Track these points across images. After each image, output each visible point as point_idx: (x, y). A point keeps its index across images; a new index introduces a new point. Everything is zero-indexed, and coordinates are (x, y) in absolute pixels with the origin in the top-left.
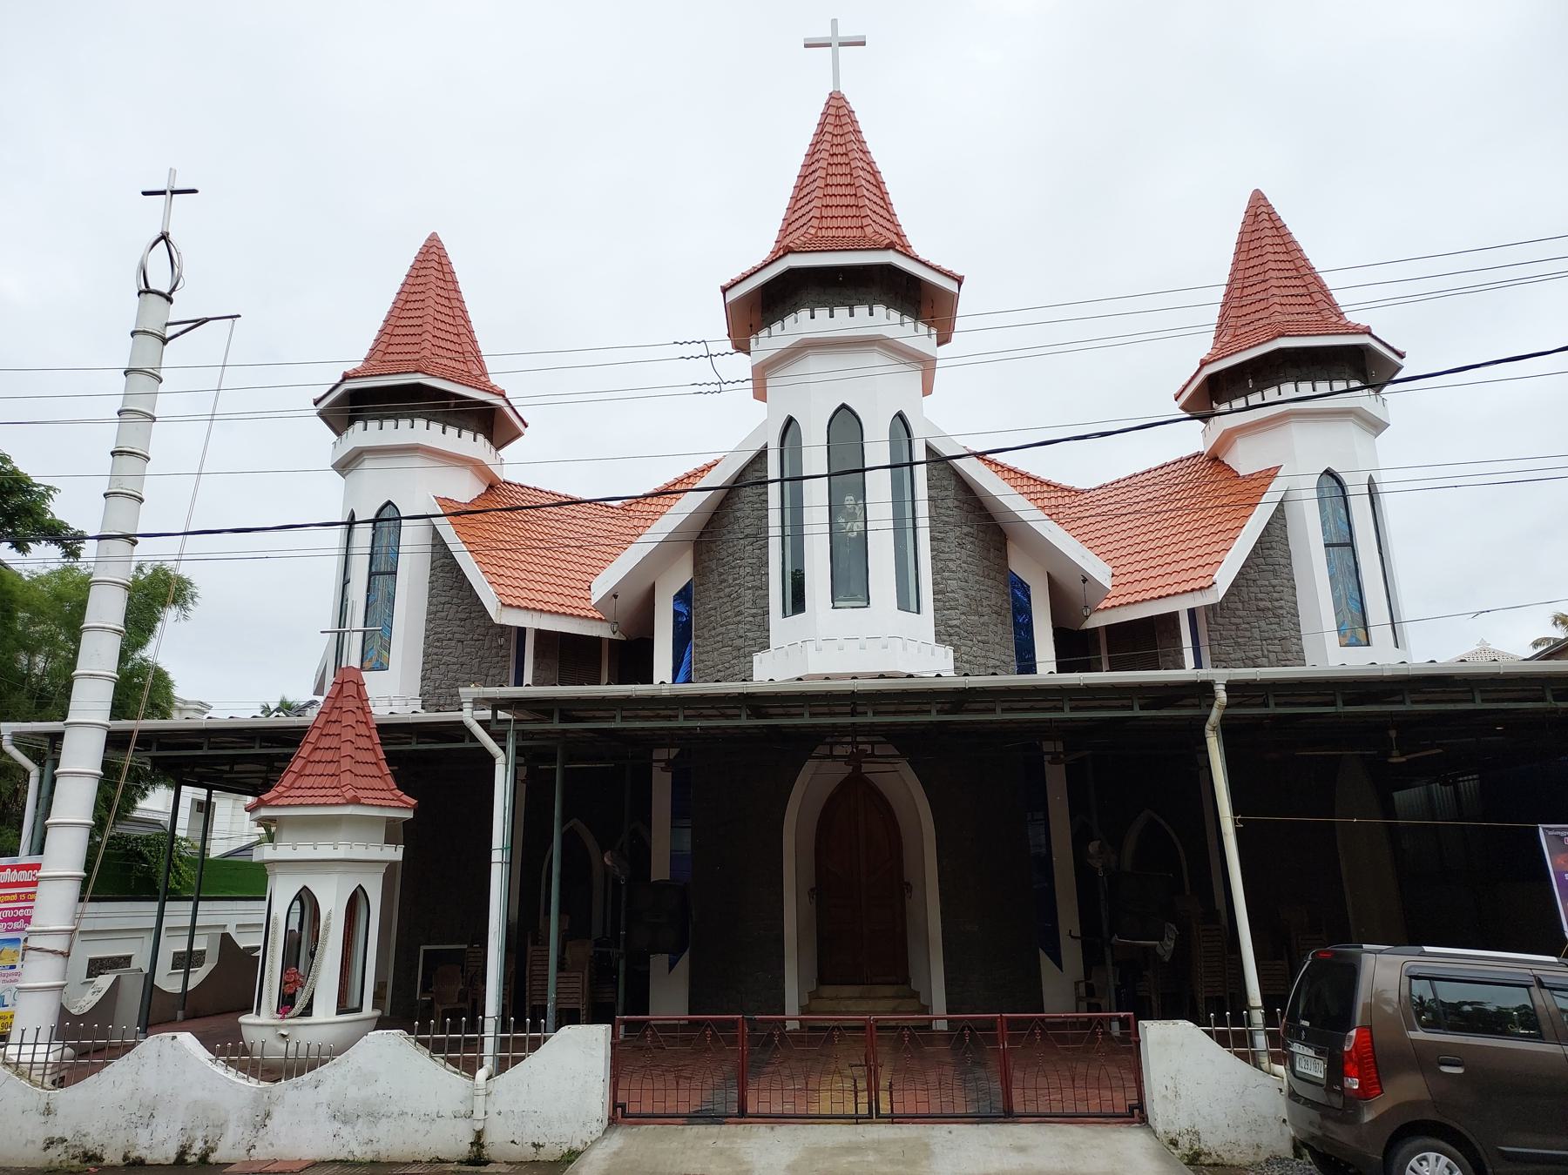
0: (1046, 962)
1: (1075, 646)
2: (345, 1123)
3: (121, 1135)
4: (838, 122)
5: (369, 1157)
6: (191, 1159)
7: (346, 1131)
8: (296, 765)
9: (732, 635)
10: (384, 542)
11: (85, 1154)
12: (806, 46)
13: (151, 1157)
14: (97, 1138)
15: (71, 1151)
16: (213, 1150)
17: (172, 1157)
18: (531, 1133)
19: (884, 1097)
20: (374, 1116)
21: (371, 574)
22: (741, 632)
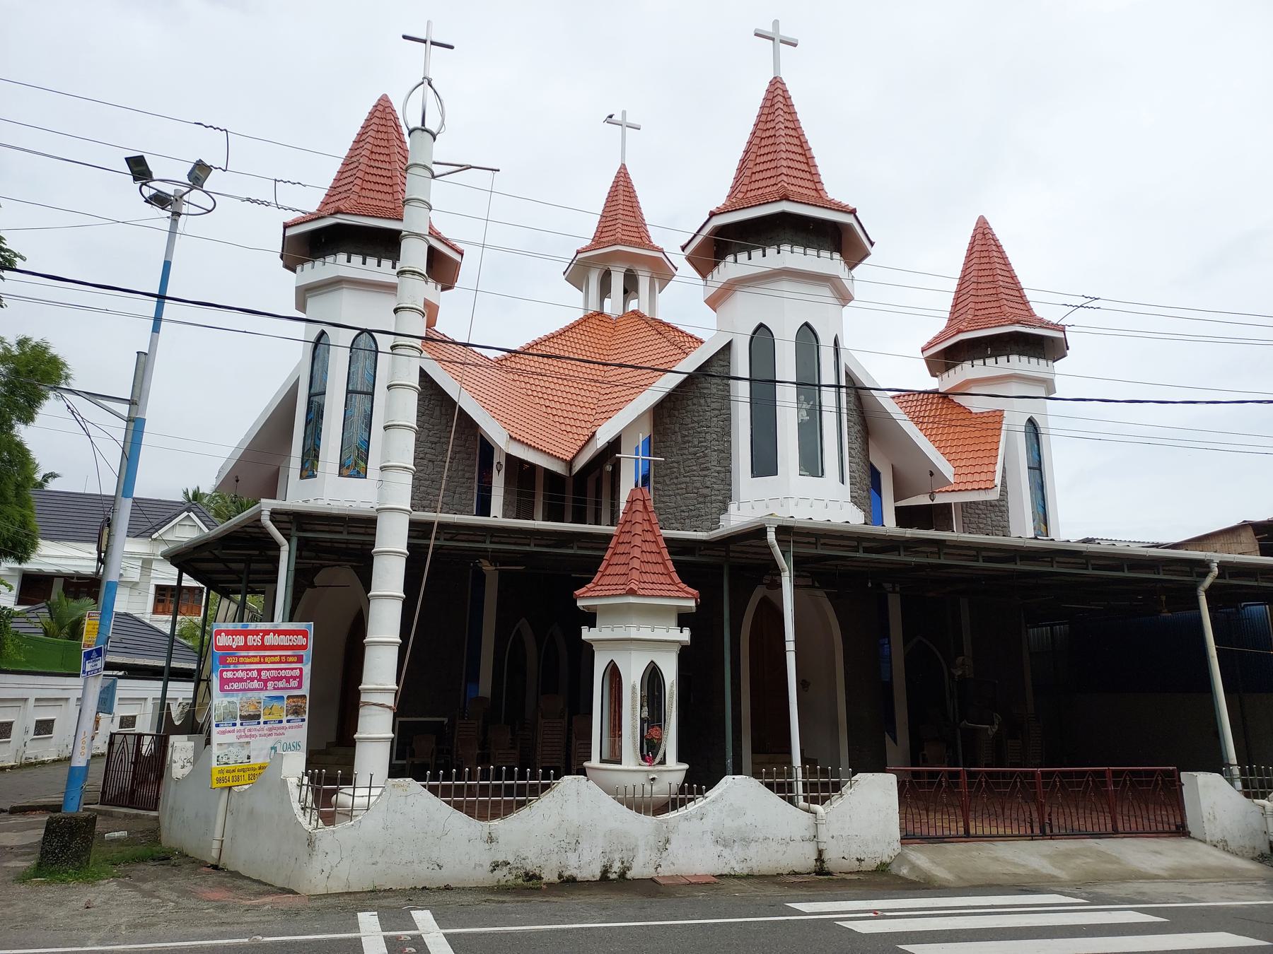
0: (888, 738)
1: (905, 517)
2: (725, 846)
3: (554, 858)
4: (777, 103)
5: (745, 872)
7: (726, 852)
9: (698, 485)
10: (360, 364)
11: (527, 874)
12: (756, 35)
13: (582, 875)
14: (535, 861)
15: (514, 872)
17: (598, 875)
18: (855, 851)
19: (972, 824)
20: (746, 841)
21: (348, 392)
22: (708, 484)
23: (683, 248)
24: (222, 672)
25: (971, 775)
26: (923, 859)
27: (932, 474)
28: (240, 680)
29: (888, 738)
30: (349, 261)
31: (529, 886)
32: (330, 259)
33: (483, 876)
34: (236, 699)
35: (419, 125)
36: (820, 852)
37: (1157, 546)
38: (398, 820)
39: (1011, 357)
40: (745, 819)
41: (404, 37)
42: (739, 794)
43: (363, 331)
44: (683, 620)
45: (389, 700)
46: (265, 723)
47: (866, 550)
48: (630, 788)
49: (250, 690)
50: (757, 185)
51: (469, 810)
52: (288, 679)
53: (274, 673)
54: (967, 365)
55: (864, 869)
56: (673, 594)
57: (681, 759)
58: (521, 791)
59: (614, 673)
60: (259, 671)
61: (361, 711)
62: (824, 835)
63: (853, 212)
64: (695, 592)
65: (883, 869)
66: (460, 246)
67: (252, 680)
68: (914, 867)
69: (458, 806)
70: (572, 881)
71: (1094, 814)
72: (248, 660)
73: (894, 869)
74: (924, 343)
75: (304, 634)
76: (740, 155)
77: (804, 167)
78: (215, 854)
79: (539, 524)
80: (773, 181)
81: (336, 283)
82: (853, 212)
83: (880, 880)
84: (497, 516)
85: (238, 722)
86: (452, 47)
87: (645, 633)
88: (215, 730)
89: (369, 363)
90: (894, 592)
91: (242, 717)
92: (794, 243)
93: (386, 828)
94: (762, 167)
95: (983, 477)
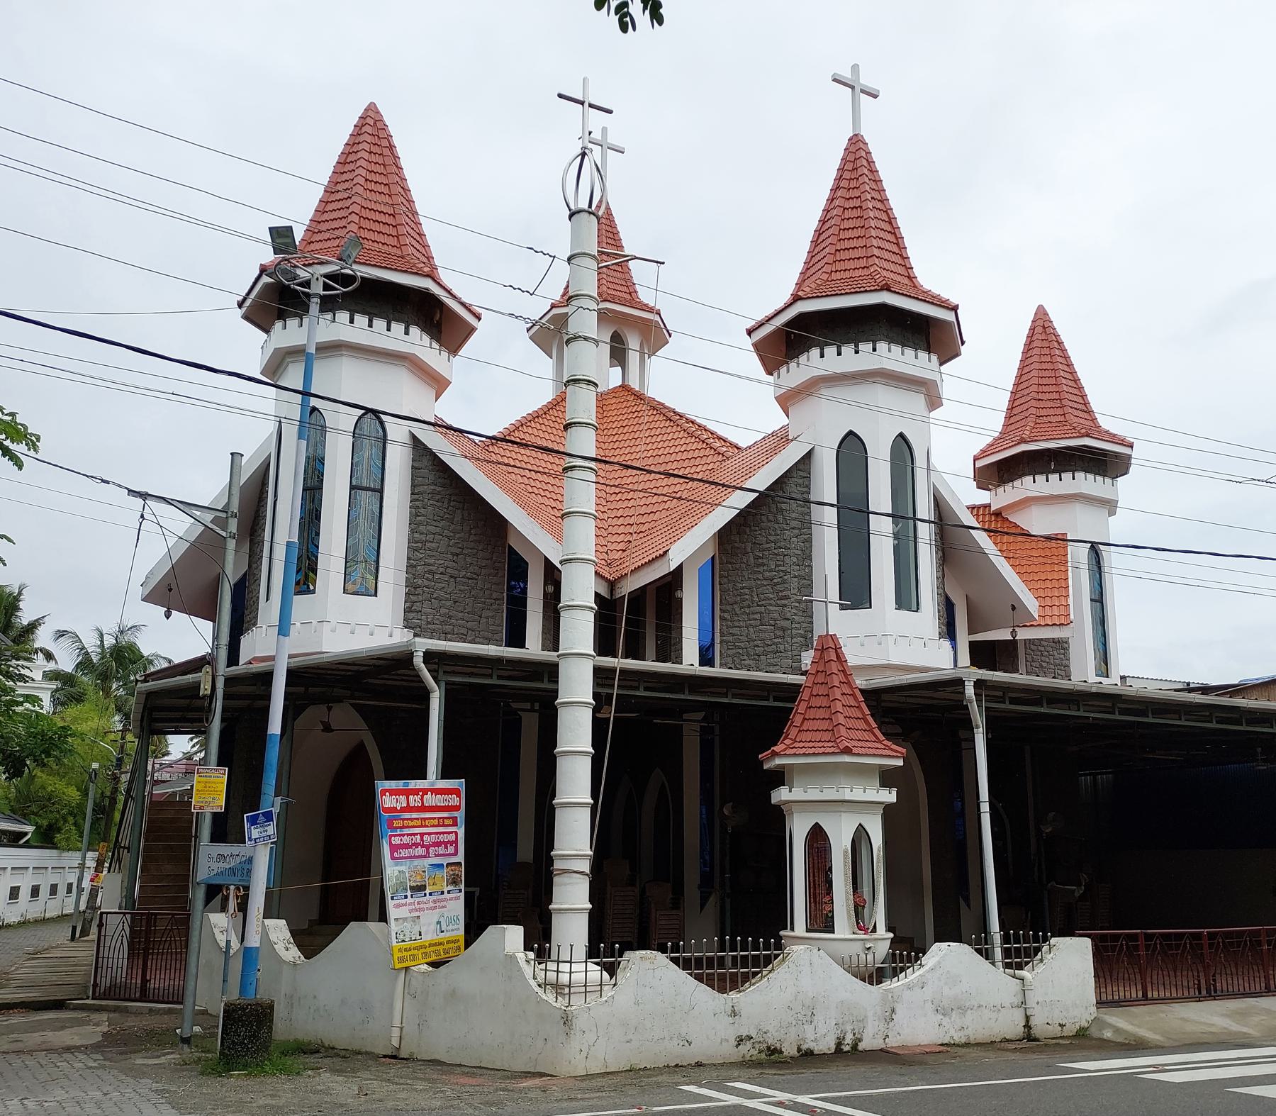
2: (944, 1015)
3: (793, 1030)
4: (857, 169)
6: (846, 1048)
7: (946, 1021)
8: (798, 720)
9: (776, 616)
11: (768, 1048)
12: (835, 80)
14: (776, 1034)
16: (860, 1040)
20: (963, 1010)
21: (352, 488)
23: (750, 332)
24: (391, 836)
25: (1149, 937)
26: (1122, 1022)
27: (1014, 608)
28: (406, 846)
29: (962, 902)
30: (352, 321)
31: (771, 1061)
32: (1017, 483)
33: (728, 1051)
34: (404, 867)
35: (586, 207)
36: (1027, 1018)
37: (1206, 690)
38: (656, 999)
39: (1076, 474)
40: (958, 988)
41: (560, 96)
42: (947, 960)
43: (368, 410)
44: (887, 778)
45: (585, 866)
46: (430, 894)
47: (1013, 701)
48: (855, 959)
49: (415, 857)
50: (842, 266)
51: (709, 981)
52: (446, 844)
53: (434, 838)
54: (1028, 479)
55: (1065, 1034)
56: (879, 752)
57: (889, 929)
58: (756, 962)
59: (817, 837)
60: (422, 835)
61: (556, 880)
62: (1031, 1003)
63: (955, 309)
64: (904, 751)
65: (1082, 1034)
66: (479, 310)
67: (416, 845)
68: (1117, 1030)
69: (699, 978)
70: (809, 1053)
71: (1121, 984)
72: (411, 824)
73: (1094, 1032)
74: (976, 451)
75: (455, 792)
76: (814, 224)
77: (895, 249)
78: (395, 1042)
79: (648, 665)
80: (862, 263)
81: (333, 349)
82: (955, 309)
83: (1083, 1041)
84: (690, 660)
85: (409, 894)
86: (610, 112)
87: (857, 794)
88: (390, 904)
89: (376, 451)
90: (532, 710)
91: (412, 889)
92: (891, 341)
93: (637, 1003)
94: (847, 244)
95: (1056, 611)
